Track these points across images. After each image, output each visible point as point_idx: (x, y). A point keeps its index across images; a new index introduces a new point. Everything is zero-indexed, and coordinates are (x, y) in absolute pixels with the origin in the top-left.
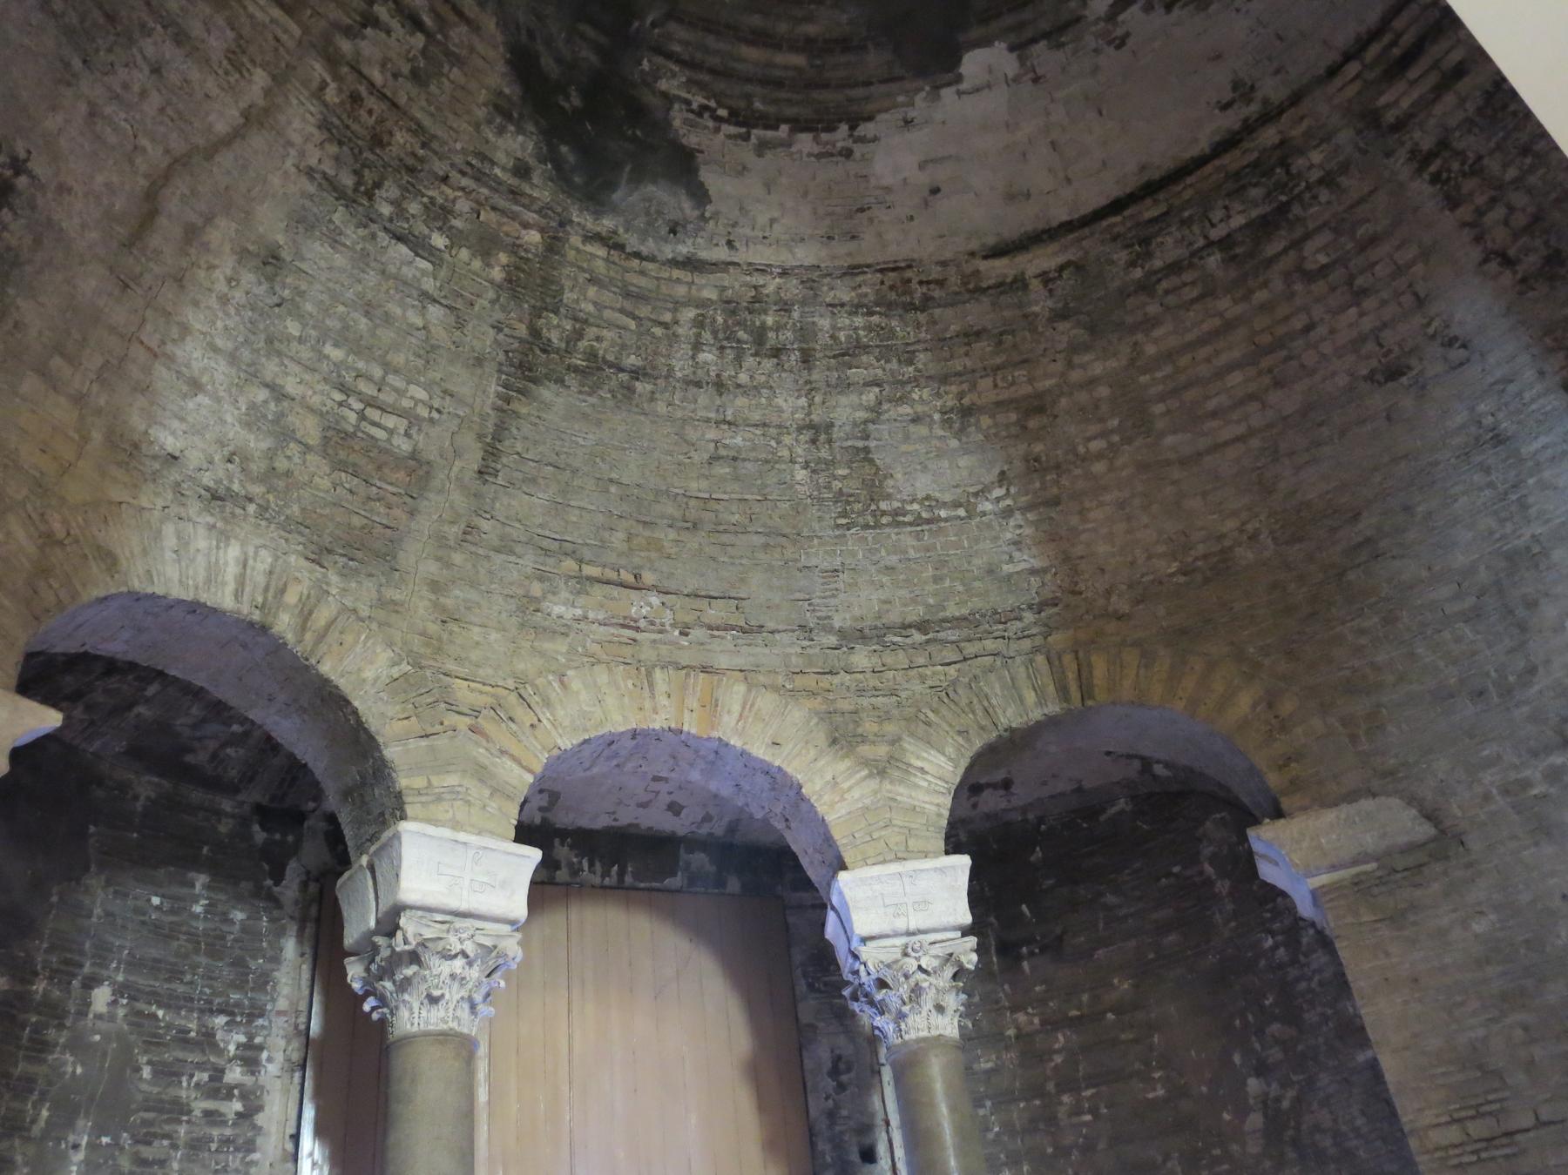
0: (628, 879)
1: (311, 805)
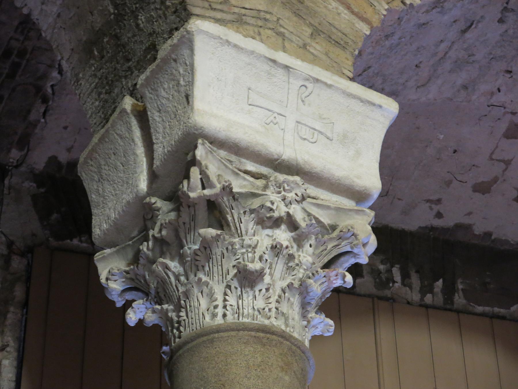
0: (459, 300)
1: (15, 154)
